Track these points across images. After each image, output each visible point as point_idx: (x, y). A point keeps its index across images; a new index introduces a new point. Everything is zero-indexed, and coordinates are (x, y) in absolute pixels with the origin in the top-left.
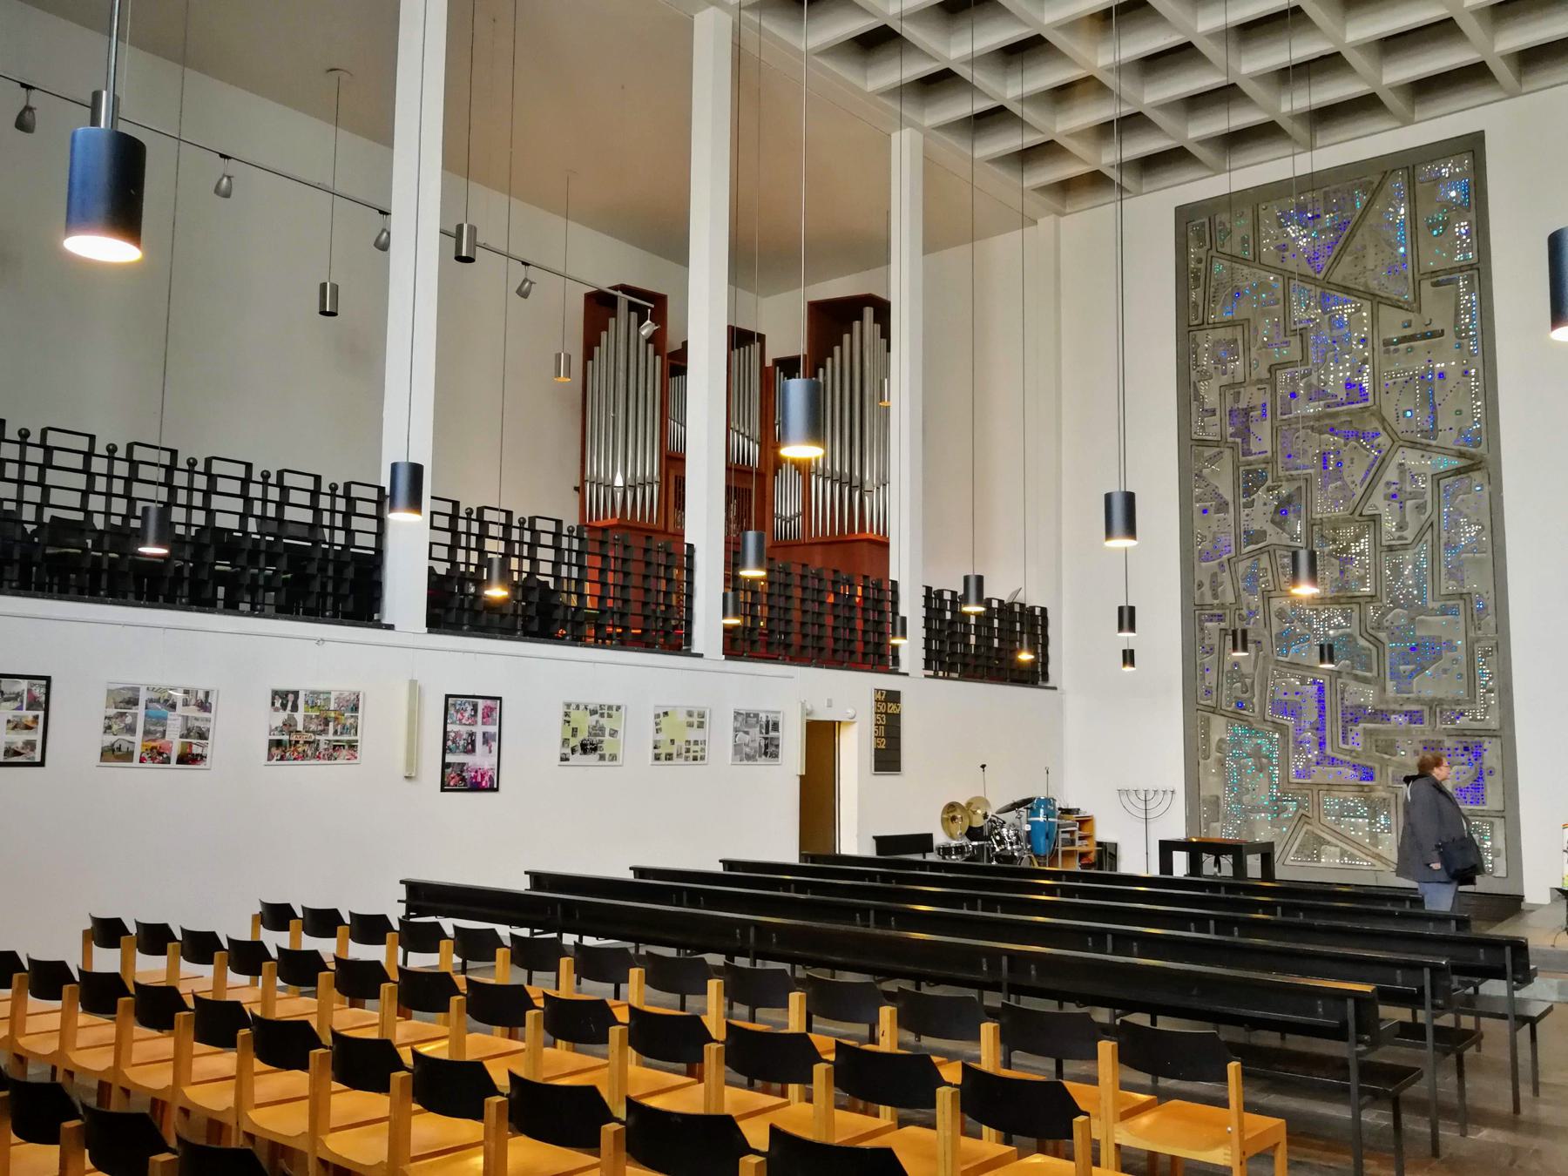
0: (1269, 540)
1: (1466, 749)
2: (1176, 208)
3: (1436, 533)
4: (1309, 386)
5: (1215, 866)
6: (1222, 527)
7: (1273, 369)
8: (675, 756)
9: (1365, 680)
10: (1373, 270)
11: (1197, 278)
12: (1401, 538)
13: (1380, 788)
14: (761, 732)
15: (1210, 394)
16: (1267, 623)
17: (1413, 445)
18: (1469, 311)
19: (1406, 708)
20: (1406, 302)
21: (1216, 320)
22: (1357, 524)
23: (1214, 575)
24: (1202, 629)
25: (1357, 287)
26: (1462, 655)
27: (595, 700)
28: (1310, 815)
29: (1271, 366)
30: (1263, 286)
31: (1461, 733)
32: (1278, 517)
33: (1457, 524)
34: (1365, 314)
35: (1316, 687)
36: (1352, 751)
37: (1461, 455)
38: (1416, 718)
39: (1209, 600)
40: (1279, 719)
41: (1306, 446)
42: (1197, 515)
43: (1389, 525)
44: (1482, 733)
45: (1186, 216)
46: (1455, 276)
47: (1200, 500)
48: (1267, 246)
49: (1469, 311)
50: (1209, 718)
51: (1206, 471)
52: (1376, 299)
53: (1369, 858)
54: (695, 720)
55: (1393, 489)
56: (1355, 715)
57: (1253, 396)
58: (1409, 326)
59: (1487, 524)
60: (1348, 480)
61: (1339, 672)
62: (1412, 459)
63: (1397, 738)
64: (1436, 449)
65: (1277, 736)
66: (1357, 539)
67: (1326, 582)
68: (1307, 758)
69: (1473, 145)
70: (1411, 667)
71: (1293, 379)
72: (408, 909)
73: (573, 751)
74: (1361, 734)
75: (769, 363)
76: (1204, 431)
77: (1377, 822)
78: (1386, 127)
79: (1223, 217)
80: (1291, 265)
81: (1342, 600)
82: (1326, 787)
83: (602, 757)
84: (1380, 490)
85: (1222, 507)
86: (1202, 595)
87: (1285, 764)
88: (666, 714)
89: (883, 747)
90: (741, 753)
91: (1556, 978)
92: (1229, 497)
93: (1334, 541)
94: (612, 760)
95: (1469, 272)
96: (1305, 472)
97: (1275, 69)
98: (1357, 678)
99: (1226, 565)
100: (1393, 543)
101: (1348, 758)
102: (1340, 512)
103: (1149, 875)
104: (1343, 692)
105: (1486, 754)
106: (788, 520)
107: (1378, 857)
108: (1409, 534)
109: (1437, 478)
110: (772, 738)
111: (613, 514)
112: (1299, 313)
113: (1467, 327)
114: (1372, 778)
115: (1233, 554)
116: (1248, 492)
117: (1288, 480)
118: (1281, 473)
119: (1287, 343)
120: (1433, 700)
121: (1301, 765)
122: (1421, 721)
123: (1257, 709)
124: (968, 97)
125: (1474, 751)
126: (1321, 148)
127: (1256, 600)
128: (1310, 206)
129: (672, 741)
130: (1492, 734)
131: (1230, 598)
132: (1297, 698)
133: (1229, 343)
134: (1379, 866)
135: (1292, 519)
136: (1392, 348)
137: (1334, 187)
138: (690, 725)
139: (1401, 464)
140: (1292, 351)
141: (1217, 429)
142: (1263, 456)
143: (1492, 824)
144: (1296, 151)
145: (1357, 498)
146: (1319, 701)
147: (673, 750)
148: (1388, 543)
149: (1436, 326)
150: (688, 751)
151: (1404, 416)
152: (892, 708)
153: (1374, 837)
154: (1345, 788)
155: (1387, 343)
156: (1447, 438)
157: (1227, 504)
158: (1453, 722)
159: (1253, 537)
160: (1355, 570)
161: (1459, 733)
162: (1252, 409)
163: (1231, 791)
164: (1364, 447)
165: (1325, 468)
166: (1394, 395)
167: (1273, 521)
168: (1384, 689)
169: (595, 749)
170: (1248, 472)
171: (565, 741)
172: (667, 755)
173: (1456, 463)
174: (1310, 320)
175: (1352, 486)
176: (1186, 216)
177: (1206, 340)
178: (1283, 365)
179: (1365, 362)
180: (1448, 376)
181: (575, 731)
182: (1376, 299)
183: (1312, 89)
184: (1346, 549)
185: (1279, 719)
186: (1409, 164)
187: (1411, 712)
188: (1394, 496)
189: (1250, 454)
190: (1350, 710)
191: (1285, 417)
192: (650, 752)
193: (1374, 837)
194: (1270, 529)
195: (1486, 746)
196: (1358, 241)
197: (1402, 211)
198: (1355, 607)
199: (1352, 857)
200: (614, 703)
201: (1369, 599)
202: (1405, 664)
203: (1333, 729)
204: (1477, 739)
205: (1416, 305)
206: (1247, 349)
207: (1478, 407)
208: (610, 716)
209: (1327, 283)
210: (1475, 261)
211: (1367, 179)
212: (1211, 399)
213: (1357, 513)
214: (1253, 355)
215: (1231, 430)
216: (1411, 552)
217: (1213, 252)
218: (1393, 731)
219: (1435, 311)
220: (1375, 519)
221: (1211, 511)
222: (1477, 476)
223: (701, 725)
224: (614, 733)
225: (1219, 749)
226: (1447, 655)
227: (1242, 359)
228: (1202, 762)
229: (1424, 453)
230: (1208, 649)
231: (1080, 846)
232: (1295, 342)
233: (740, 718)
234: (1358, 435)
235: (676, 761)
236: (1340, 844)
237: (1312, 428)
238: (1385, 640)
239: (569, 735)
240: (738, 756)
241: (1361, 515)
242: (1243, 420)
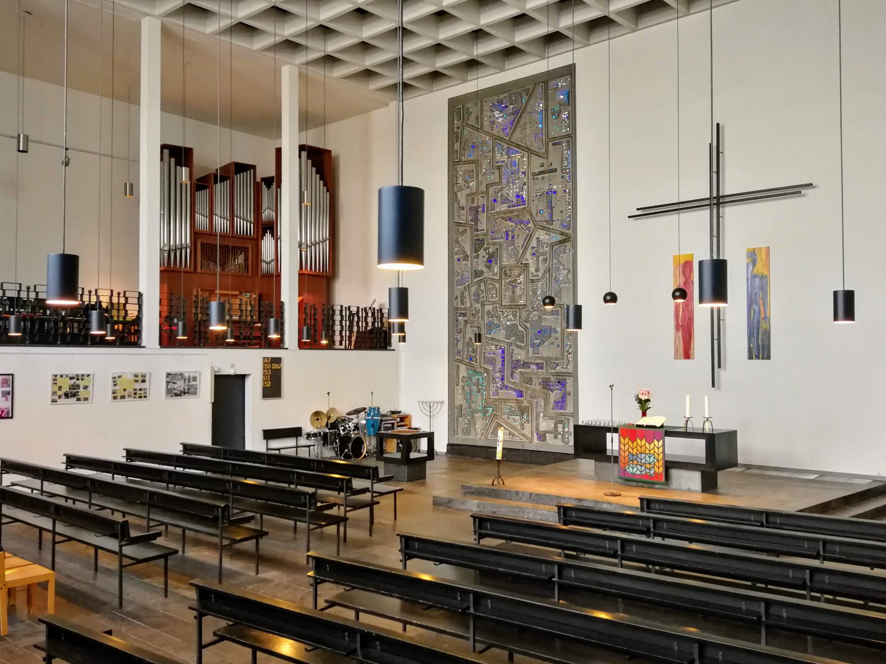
0: (485, 275)
1: (559, 382)
2: (449, 99)
3: (551, 273)
4: (502, 196)
5: (11, 483)
6: (465, 267)
7: (487, 187)
8: (126, 396)
9: (520, 347)
10: (527, 134)
11: (457, 138)
12: (537, 276)
13: (525, 401)
14: (185, 382)
15: (462, 197)
16: (483, 318)
17: (543, 228)
18: (567, 159)
19: (537, 361)
20: (542, 153)
21: (465, 160)
22: (520, 268)
23: (462, 293)
24: (457, 321)
25: (521, 144)
26: (559, 335)
27: (73, 372)
28: (497, 414)
29: (487, 185)
30: (484, 143)
31: (558, 374)
32: (488, 263)
33: (559, 269)
34: (525, 159)
35: (501, 350)
36: (515, 383)
37: (562, 234)
38: (540, 366)
39: (460, 306)
40: (486, 366)
41: (500, 228)
42: (456, 261)
43: (532, 269)
44: (566, 374)
45: (453, 103)
46: (562, 140)
47: (457, 254)
48: (486, 121)
49: (567, 159)
50: (459, 366)
51: (460, 239)
52: (529, 151)
53: (520, 436)
54: (140, 379)
55: (534, 251)
56: (516, 365)
57: (481, 201)
58: (543, 166)
59: (571, 269)
60: (517, 245)
61: (511, 343)
62: (542, 235)
63: (533, 377)
64: (552, 231)
65: (485, 375)
66: (519, 275)
67: (507, 297)
68: (497, 386)
69: (569, 71)
70: (538, 341)
71: (495, 192)
72: (67, 466)
73: (60, 397)
74: (519, 374)
75: (258, 180)
76: (459, 218)
77: (523, 418)
78: (531, 61)
79: (469, 105)
80: (495, 132)
81: (513, 307)
82: (504, 401)
83: (79, 400)
84: (529, 252)
85: (466, 258)
86: (457, 303)
87: (488, 389)
88: (120, 377)
89: (269, 386)
90: (172, 393)
91: (477, 500)
92: (469, 253)
93: (510, 276)
94: (85, 400)
95: (568, 139)
96: (499, 240)
97: (467, 32)
98: (517, 346)
99: (467, 288)
100: (534, 278)
101: (513, 386)
102: (513, 262)
103: (309, 458)
104: (512, 353)
105: (567, 385)
106: (268, 263)
107: (524, 435)
108: (540, 274)
109: (552, 245)
110: (192, 385)
111: (164, 265)
112: (498, 157)
113: (566, 168)
114: (521, 396)
115: (470, 282)
116: (476, 251)
117: (493, 245)
118: (490, 241)
119: (494, 173)
120: (548, 357)
121: (494, 390)
122: (542, 368)
123: (478, 361)
124: (304, 53)
125: (562, 383)
126: (470, 81)
127: (478, 306)
128: (504, 101)
129: (125, 390)
130: (569, 375)
131: (468, 305)
132: (494, 356)
133: (470, 172)
134: (524, 440)
135: (493, 265)
136: (536, 177)
137: (515, 91)
138: (137, 381)
139: (538, 238)
140: (494, 178)
141: (464, 217)
142: (483, 232)
143: (569, 419)
144: (575, 47)
145: (520, 254)
146: (502, 358)
147: (126, 394)
148: (531, 278)
149: (553, 167)
150: (135, 394)
151: (540, 213)
152: (275, 366)
153: (522, 425)
154: (512, 401)
155: (534, 174)
156: (556, 225)
157: (468, 256)
158: (555, 369)
159: (478, 273)
160: (518, 291)
161: (557, 374)
162: (478, 207)
163: (467, 402)
164: (523, 228)
165: (507, 239)
166: (536, 202)
167: (486, 266)
168: (528, 352)
169: (74, 396)
170: (476, 240)
171: (54, 393)
172: (121, 396)
173: (559, 238)
174: (503, 162)
175: (518, 248)
176: (453, 103)
177: (461, 169)
178: (492, 184)
179: (525, 184)
180: (558, 193)
181: (60, 388)
182: (529, 151)
183: (479, 46)
184: (515, 281)
185: (486, 366)
186: (545, 80)
187: (538, 364)
188: (534, 254)
189: (478, 230)
190: (515, 362)
191: (492, 212)
192: (110, 396)
193: (522, 425)
194: (485, 270)
195: (568, 381)
196: (522, 121)
197: (541, 105)
198: (518, 310)
199: (513, 435)
200: (85, 372)
201: (523, 307)
202: (537, 339)
203: (507, 373)
204: (564, 377)
205: (546, 155)
206: (477, 176)
207: (570, 209)
208: (82, 379)
209: (510, 143)
210: (570, 133)
211: (526, 87)
212: (463, 202)
213: (520, 262)
214: (480, 179)
215: (470, 218)
216: (540, 283)
217: (464, 124)
218: (531, 373)
219: (554, 159)
220: (526, 266)
221: (461, 260)
222: (568, 245)
223: (144, 381)
224: (86, 387)
225: (462, 381)
226: (554, 335)
227: (475, 181)
228: (456, 387)
229: (547, 232)
230: (459, 331)
231: (398, 430)
232: (497, 172)
233: (170, 376)
234: (521, 222)
235: (127, 399)
236: (510, 429)
237: (503, 218)
238: (529, 328)
239: (56, 389)
240: (170, 395)
241: (521, 264)
242: (475, 211)
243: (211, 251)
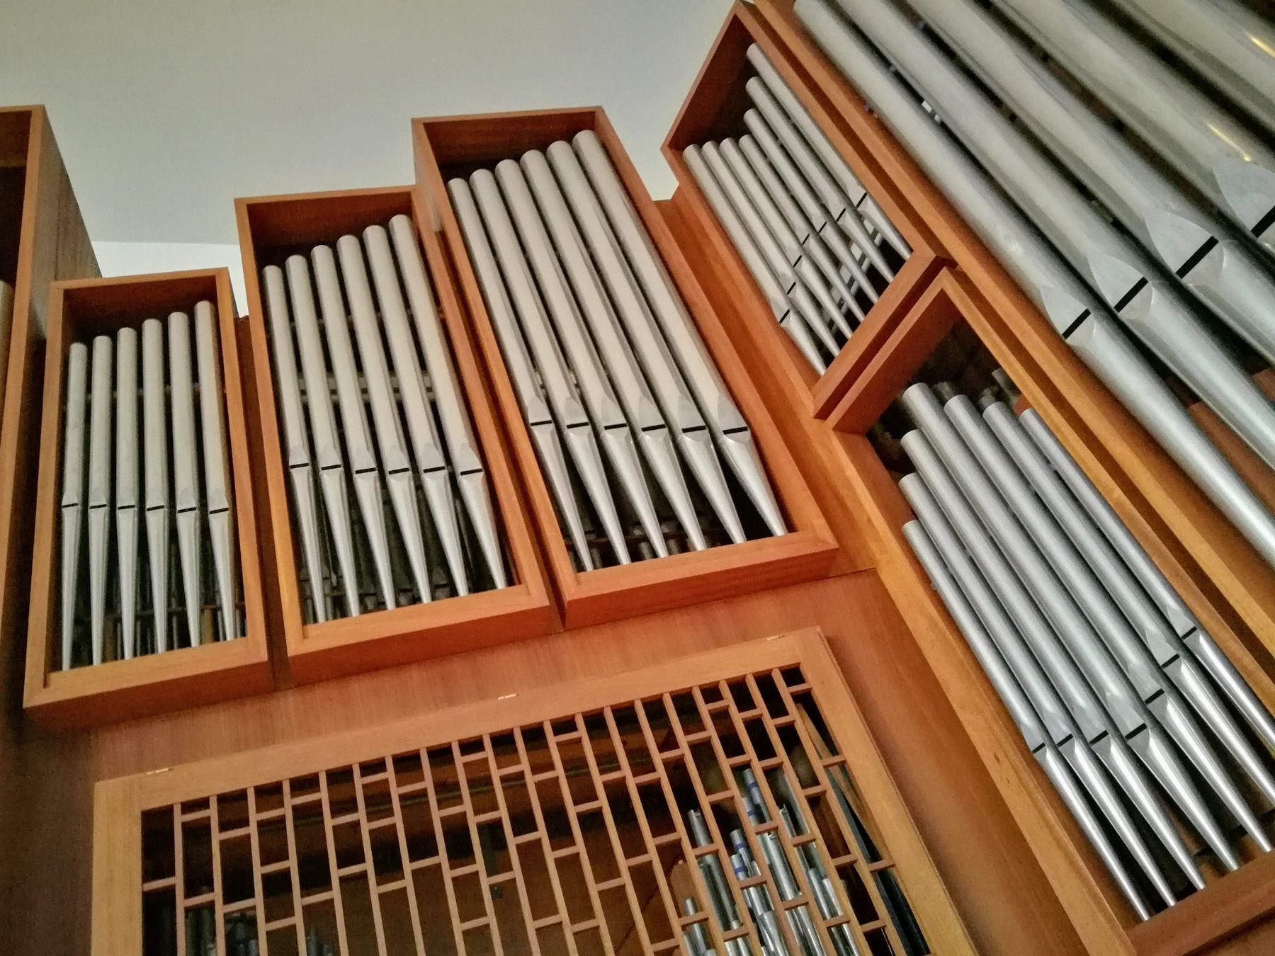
243: (605, 867)
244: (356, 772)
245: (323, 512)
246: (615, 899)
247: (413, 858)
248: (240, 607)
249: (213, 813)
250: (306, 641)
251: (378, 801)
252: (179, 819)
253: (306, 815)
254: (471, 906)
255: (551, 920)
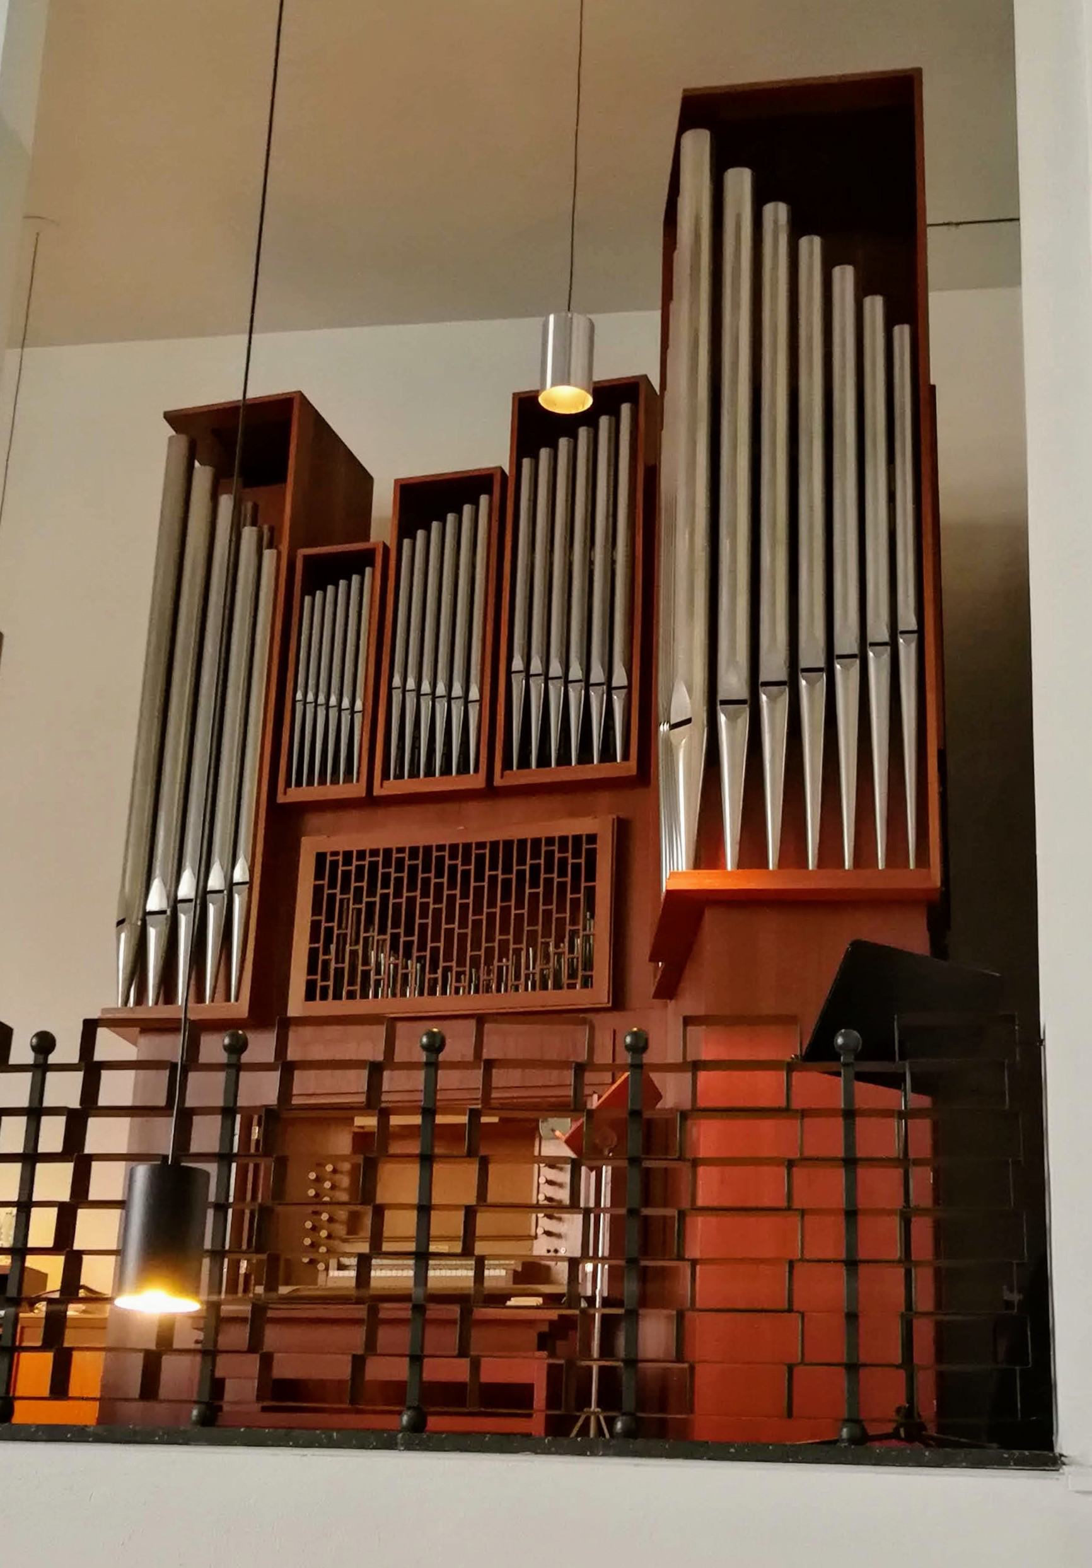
243: (478, 910)
244: (394, 851)
245: (567, 360)
246: (477, 924)
247: (357, 860)
248: (358, 773)
249: (340, 858)
250: (383, 789)
251: (400, 863)
252: (329, 858)
253: (374, 866)
254: (424, 915)
255: (462, 931)
